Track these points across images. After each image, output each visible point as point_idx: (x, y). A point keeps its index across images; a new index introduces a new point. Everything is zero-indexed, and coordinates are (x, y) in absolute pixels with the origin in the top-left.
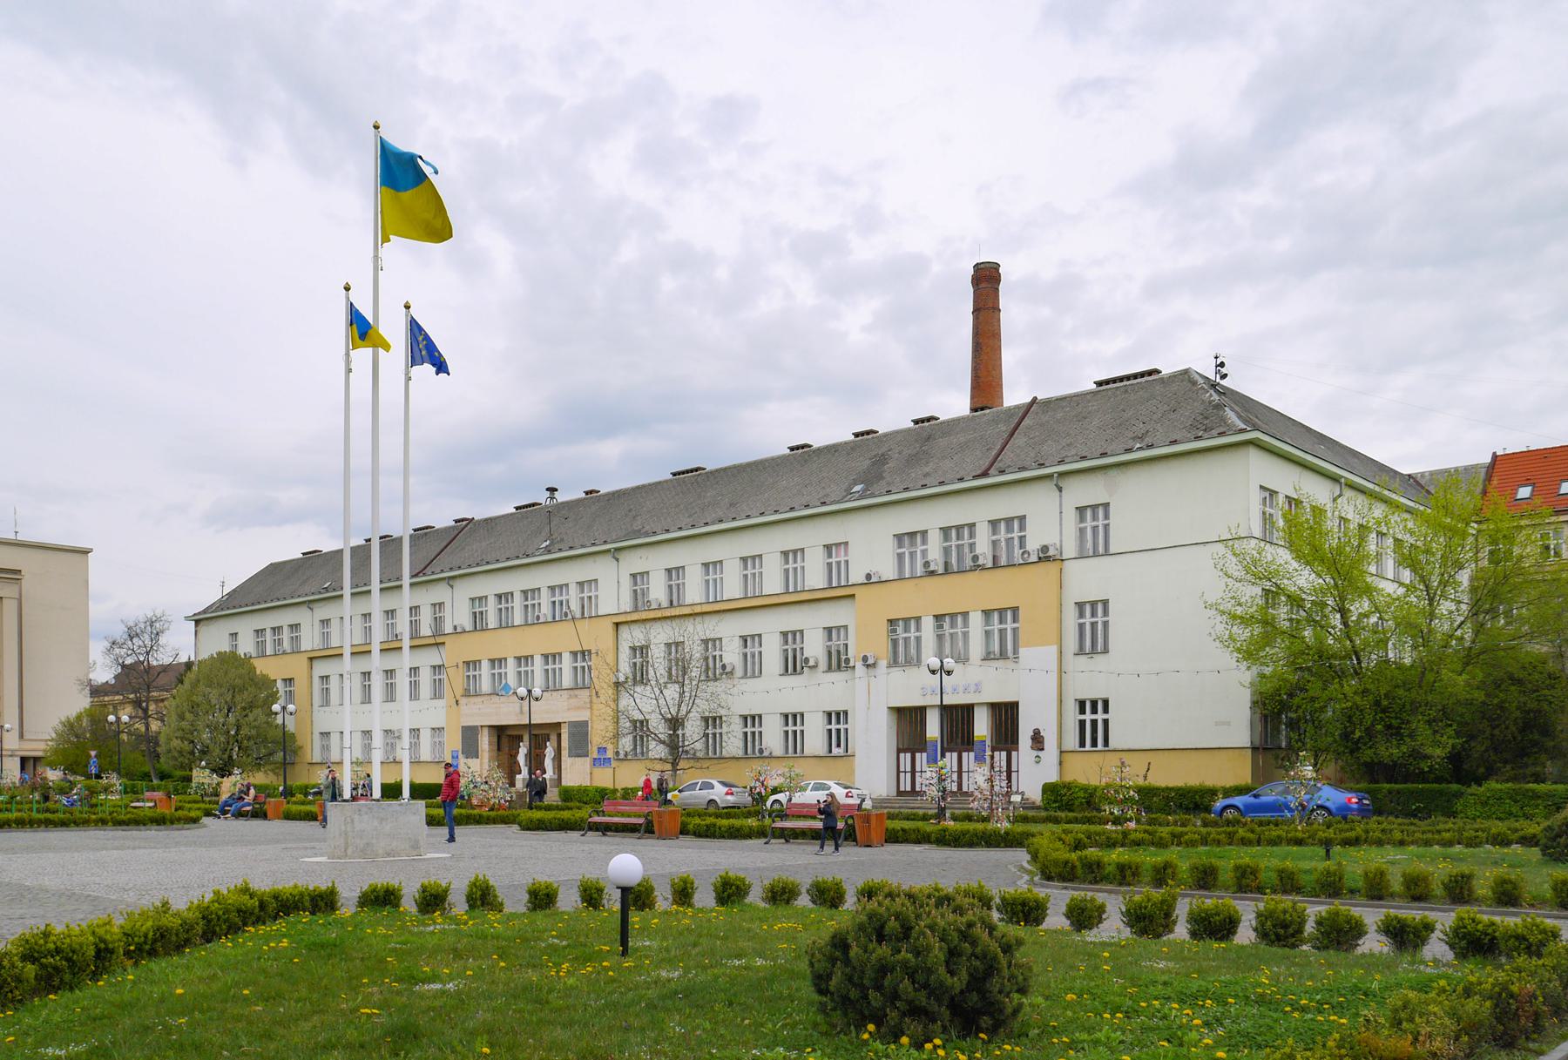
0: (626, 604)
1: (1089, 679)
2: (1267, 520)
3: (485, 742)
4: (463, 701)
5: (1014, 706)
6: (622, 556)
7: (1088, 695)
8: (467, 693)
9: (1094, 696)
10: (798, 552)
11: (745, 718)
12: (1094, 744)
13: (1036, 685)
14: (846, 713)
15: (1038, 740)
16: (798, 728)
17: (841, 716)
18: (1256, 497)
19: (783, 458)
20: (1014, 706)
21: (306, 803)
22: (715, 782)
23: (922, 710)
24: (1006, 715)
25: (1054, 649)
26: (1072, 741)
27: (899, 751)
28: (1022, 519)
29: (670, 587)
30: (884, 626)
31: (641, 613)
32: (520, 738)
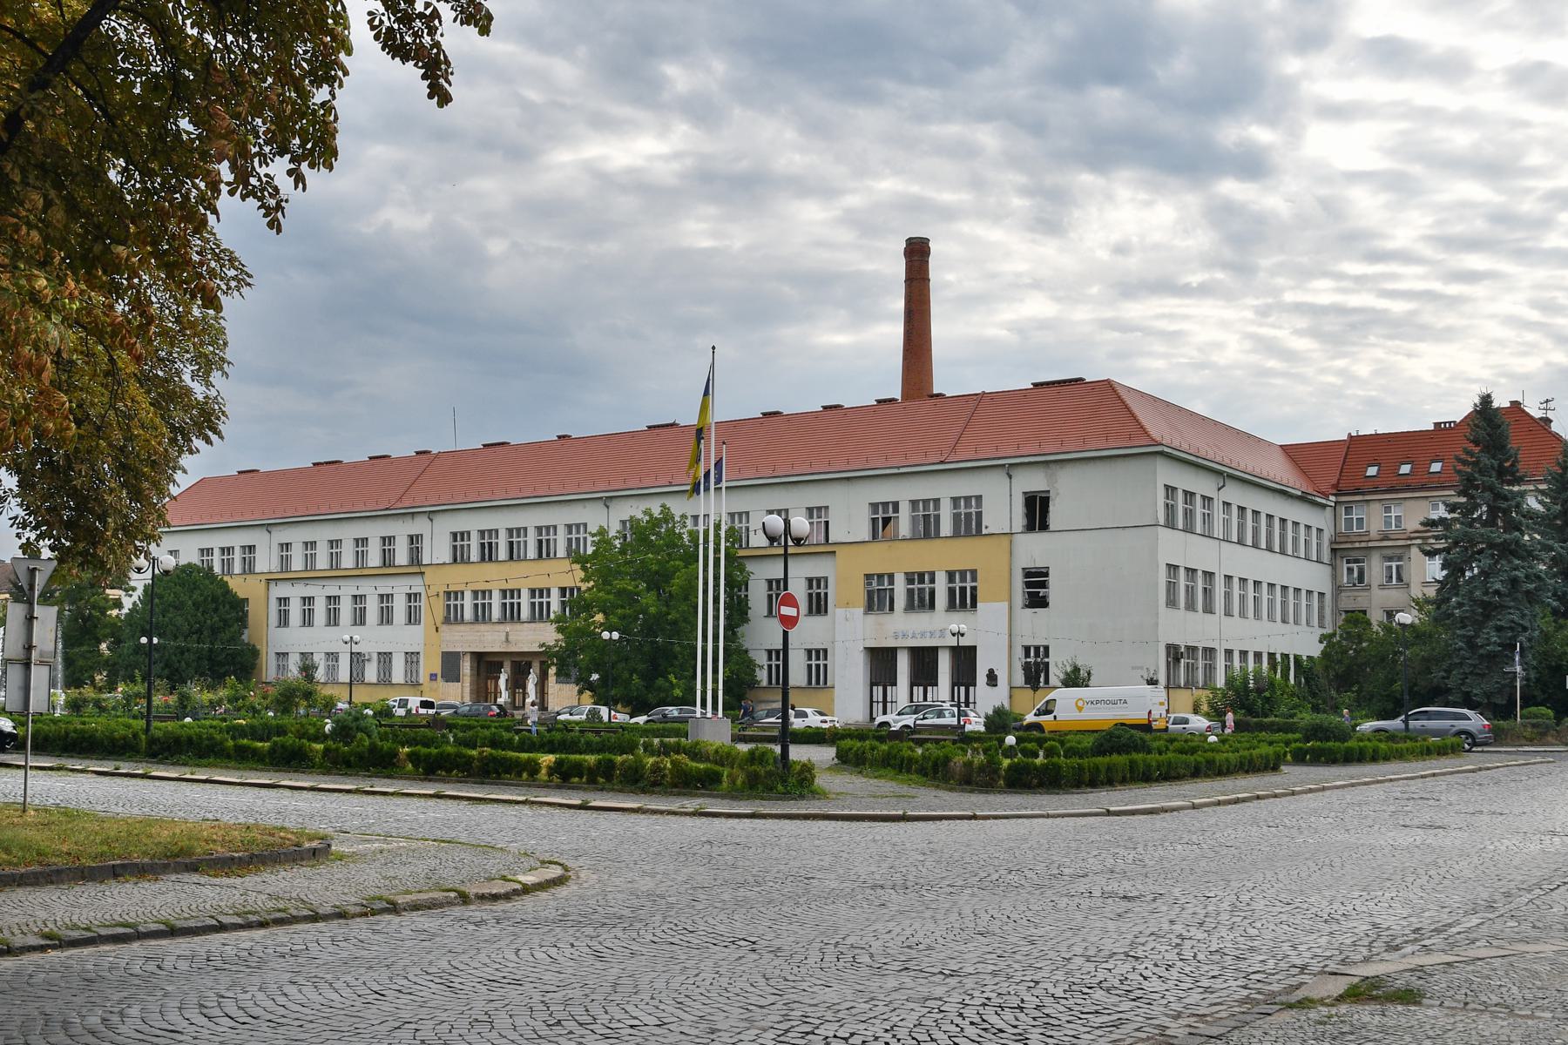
0: (275, 565)
1: (1035, 627)
2: (1170, 509)
3: (466, 667)
4: (444, 628)
5: (972, 650)
6: (612, 505)
7: (1182, 641)
8: (447, 621)
9: (1036, 643)
10: (364, 541)
11: (809, 652)
12: (818, 682)
13: (993, 630)
14: (825, 651)
15: (992, 679)
16: (821, 662)
17: (821, 653)
18: (1161, 493)
19: (1023, 393)
20: (972, 650)
21: (1149, 752)
22: (809, 711)
23: (934, 651)
24: (965, 658)
25: (1006, 604)
26: (1019, 679)
27: (872, 684)
28: (979, 498)
29: (455, 547)
30: (861, 581)
31: (285, 575)
32: (529, 665)
